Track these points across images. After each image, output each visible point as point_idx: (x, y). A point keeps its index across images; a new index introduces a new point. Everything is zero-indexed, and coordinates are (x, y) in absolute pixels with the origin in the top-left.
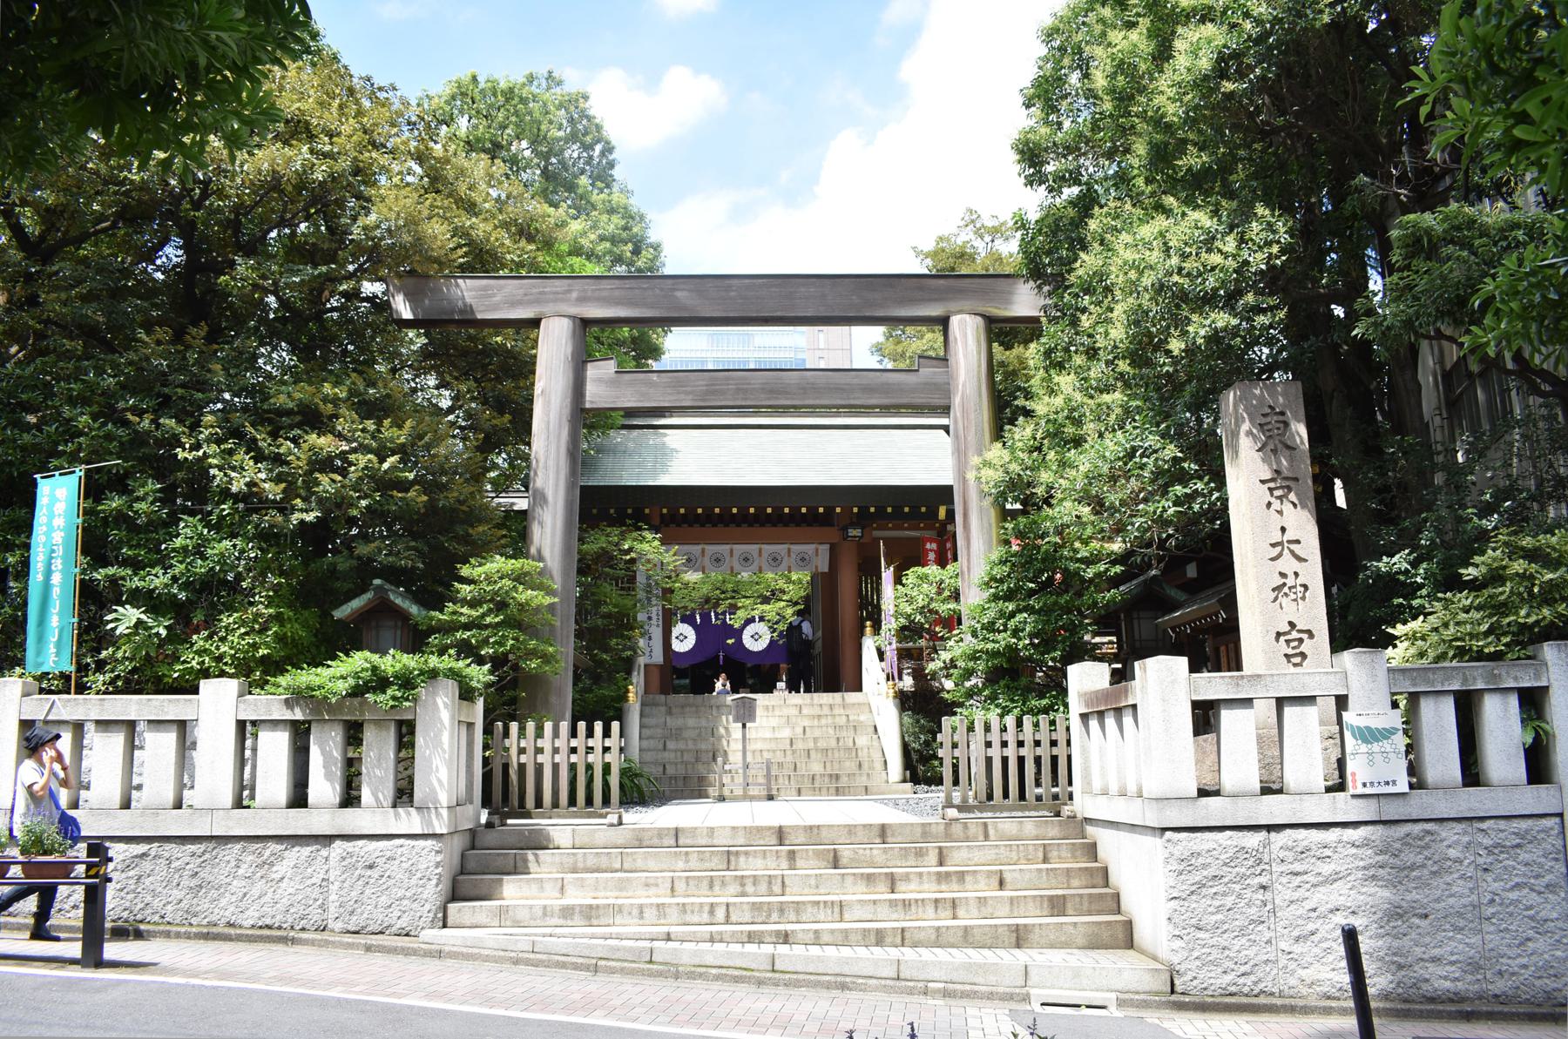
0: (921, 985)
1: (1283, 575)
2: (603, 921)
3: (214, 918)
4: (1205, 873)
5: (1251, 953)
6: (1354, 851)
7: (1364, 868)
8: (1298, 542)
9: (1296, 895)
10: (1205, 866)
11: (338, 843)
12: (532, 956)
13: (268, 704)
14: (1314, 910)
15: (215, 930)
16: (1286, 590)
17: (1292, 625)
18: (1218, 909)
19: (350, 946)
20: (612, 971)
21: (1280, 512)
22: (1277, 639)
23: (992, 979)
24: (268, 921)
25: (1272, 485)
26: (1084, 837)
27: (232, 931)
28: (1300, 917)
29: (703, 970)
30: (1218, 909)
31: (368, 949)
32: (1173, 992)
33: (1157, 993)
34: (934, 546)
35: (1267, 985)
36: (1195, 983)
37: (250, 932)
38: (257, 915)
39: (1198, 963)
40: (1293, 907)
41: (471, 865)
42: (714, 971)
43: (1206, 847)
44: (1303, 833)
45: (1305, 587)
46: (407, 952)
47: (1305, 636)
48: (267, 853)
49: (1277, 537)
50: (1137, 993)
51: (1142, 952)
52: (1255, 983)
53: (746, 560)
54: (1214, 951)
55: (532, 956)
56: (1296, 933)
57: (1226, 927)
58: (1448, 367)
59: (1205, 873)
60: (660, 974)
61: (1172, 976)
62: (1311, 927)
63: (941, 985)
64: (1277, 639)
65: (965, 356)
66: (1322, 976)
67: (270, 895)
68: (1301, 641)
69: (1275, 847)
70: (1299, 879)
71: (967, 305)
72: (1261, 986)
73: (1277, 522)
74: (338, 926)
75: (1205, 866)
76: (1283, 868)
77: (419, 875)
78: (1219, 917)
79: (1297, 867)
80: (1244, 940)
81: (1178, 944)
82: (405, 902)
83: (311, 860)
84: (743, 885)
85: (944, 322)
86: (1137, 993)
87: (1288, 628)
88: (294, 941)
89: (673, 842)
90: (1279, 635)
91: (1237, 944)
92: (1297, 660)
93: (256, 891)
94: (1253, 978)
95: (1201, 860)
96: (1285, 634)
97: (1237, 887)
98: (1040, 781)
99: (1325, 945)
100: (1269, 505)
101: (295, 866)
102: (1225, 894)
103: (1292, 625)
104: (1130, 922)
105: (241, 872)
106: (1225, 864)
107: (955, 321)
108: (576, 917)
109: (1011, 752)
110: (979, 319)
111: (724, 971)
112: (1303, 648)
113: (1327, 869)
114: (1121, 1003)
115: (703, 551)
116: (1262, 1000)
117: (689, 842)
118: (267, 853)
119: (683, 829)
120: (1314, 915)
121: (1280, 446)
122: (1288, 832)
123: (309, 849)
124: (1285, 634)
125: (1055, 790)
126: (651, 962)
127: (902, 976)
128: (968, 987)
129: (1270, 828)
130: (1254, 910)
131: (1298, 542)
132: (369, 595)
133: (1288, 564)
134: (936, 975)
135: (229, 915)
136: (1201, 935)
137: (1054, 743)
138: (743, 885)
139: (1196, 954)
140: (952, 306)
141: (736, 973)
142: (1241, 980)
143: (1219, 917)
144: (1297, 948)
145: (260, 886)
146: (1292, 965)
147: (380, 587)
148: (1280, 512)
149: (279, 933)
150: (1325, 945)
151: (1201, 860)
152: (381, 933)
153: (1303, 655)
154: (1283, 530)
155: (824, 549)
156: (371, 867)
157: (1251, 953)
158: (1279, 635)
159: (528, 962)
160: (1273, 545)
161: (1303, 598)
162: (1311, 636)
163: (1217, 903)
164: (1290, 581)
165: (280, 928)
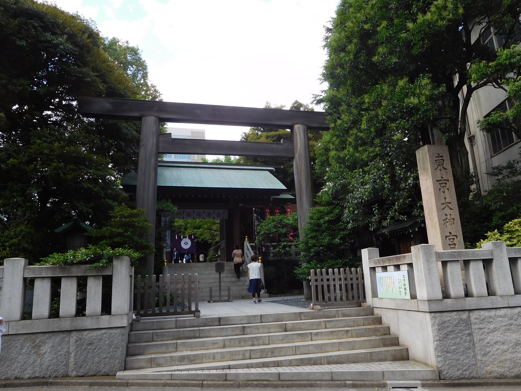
0: (343, 382)
1: (446, 215)
2: (152, 351)
3: (8, 376)
4: (448, 329)
5: (467, 361)
6: (501, 319)
7: (505, 326)
8: (450, 203)
9: (482, 337)
10: (448, 327)
11: (74, 333)
12: (172, 382)
13: (44, 269)
14: (489, 343)
15: (8, 382)
16: (447, 220)
17: (450, 233)
18: (454, 344)
19: (81, 384)
20: (209, 386)
21: (444, 192)
22: (446, 238)
23: (370, 378)
24: (37, 375)
25: (440, 182)
26: (373, 315)
27: (16, 382)
28: (484, 346)
29: (250, 382)
30: (454, 344)
31: (91, 385)
32: (440, 379)
33: (434, 380)
34: (269, 211)
35: (474, 374)
36: (447, 375)
37: (29, 381)
38: (31, 372)
39: (448, 366)
40: (481, 342)
41: (133, 339)
42: (255, 383)
43: (447, 319)
44: (482, 312)
45: (454, 219)
46: (110, 385)
47: (455, 237)
48: (38, 340)
49: (443, 201)
50: (427, 380)
51: (415, 361)
52: (470, 374)
53: (199, 214)
54: (454, 361)
55: (172, 382)
56: (483, 353)
57: (457, 351)
58: (284, 187)
59: (448, 329)
60: (231, 386)
61: (440, 373)
62: (488, 350)
63: (351, 382)
64: (446, 238)
65: (300, 140)
66: (493, 369)
67: (38, 361)
68: (454, 239)
69: (472, 318)
70: (482, 331)
72: (472, 375)
74: (74, 373)
75: (448, 327)
76: (476, 326)
77: (114, 346)
78: (455, 347)
79: (481, 326)
80: (464, 356)
81: (440, 359)
82: (107, 360)
84: (253, 341)
85: (291, 127)
86: (427, 380)
87: (449, 234)
88: (51, 384)
89: (218, 323)
90: (446, 237)
91: (462, 358)
92: (453, 246)
93: (31, 360)
94: (468, 372)
95: (446, 325)
97: (460, 335)
98: (355, 294)
99: (494, 357)
100: (440, 189)
101: (52, 346)
102: (456, 338)
104: (407, 349)
105: (24, 351)
106: (455, 326)
107: (296, 127)
108: (186, 361)
109: (343, 282)
110: (305, 126)
111: (260, 382)
112: (455, 241)
113: (492, 326)
114: (423, 386)
116: (473, 381)
117: (224, 323)
118: (38, 340)
120: (488, 345)
121: (442, 168)
122: (476, 312)
123: (60, 337)
125: (329, 295)
126: (226, 380)
127: (334, 379)
128: (362, 382)
129: (470, 310)
130: (466, 344)
131: (450, 203)
133: (447, 211)
134: (348, 378)
135: (17, 373)
136: (449, 355)
137: (357, 279)
138: (253, 341)
139: (447, 363)
141: (265, 383)
142: (465, 373)
143: (455, 347)
144: (484, 359)
145: (33, 357)
146: (482, 366)
148: (444, 192)
149: (44, 380)
150: (494, 357)
151: (446, 325)
152: (95, 375)
153: (455, 244)
154: (445, 198)
155: (227, 211)
156: (90, 344)
157: (467, 361)
158: (446, 237)
159: (170, 385)
161: (454, 223)
162: (457, 237)
163: (453, 342)
164: (449, 217)
165: (44, 377)
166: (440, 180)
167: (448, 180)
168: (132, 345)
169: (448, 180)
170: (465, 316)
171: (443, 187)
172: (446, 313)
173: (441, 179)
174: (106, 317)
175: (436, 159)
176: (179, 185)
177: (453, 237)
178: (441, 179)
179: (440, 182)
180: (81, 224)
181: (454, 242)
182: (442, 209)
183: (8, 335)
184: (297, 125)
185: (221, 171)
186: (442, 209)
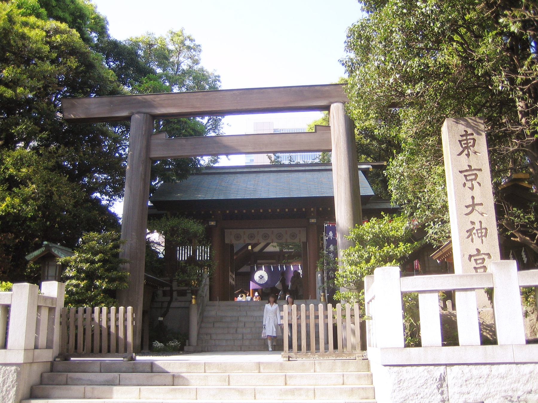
1: (473, 223)
16: (475, 231)
17: (478, 250)
25: (466, 173)
47: (486, 257)
71: (336, 99)
73: (470, 193)
83: (416, 369)
87: (476, 253)
90: (470, 256)
96: (474, 256)
100: (464, 185)
103: (478, 250)
107: (333, 107)
112: (484, 264)
115: (258, 232)
119: (263, 363)
124: (474, 256)
129: (446, 365)
132: (43, 249)
140: (332, 100)
147: (46, 246)
148: (472, 188)
154: (473, 198)
158: (470, 256)
160: (467, 207)
166: (466, 171)
167: (480, 170)
168: (44, 386)
169: (480, 170)
170: (438, 371)
171: (472, 180)
172: (409, 368)
173: (468, 168)
174: (414, 350)
175: (461, 139)
176: (222, 197)
177: (483, 256)
178: (468, 168)
179: (466, 173)
180: (53, 250)
181: (484, 264)
182: (466, 214)
183: (517, 363)
184: (335, 104)
185: (285, 175)
186: (466, 214)
